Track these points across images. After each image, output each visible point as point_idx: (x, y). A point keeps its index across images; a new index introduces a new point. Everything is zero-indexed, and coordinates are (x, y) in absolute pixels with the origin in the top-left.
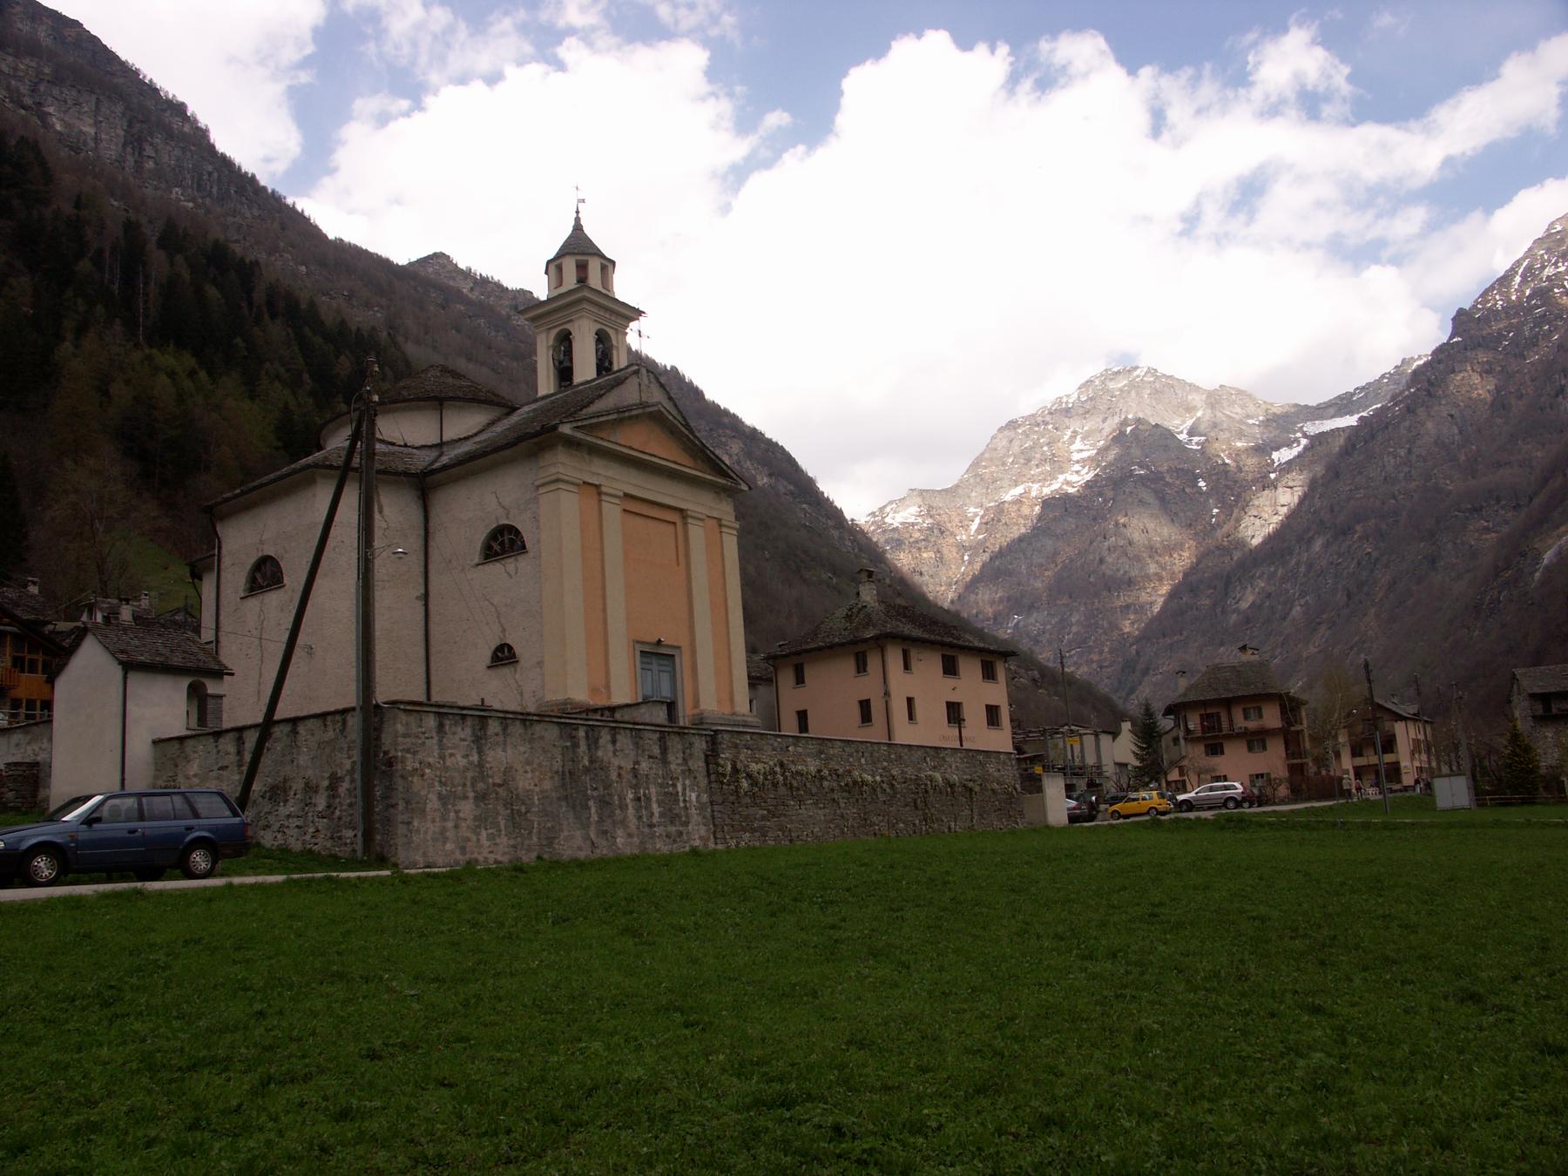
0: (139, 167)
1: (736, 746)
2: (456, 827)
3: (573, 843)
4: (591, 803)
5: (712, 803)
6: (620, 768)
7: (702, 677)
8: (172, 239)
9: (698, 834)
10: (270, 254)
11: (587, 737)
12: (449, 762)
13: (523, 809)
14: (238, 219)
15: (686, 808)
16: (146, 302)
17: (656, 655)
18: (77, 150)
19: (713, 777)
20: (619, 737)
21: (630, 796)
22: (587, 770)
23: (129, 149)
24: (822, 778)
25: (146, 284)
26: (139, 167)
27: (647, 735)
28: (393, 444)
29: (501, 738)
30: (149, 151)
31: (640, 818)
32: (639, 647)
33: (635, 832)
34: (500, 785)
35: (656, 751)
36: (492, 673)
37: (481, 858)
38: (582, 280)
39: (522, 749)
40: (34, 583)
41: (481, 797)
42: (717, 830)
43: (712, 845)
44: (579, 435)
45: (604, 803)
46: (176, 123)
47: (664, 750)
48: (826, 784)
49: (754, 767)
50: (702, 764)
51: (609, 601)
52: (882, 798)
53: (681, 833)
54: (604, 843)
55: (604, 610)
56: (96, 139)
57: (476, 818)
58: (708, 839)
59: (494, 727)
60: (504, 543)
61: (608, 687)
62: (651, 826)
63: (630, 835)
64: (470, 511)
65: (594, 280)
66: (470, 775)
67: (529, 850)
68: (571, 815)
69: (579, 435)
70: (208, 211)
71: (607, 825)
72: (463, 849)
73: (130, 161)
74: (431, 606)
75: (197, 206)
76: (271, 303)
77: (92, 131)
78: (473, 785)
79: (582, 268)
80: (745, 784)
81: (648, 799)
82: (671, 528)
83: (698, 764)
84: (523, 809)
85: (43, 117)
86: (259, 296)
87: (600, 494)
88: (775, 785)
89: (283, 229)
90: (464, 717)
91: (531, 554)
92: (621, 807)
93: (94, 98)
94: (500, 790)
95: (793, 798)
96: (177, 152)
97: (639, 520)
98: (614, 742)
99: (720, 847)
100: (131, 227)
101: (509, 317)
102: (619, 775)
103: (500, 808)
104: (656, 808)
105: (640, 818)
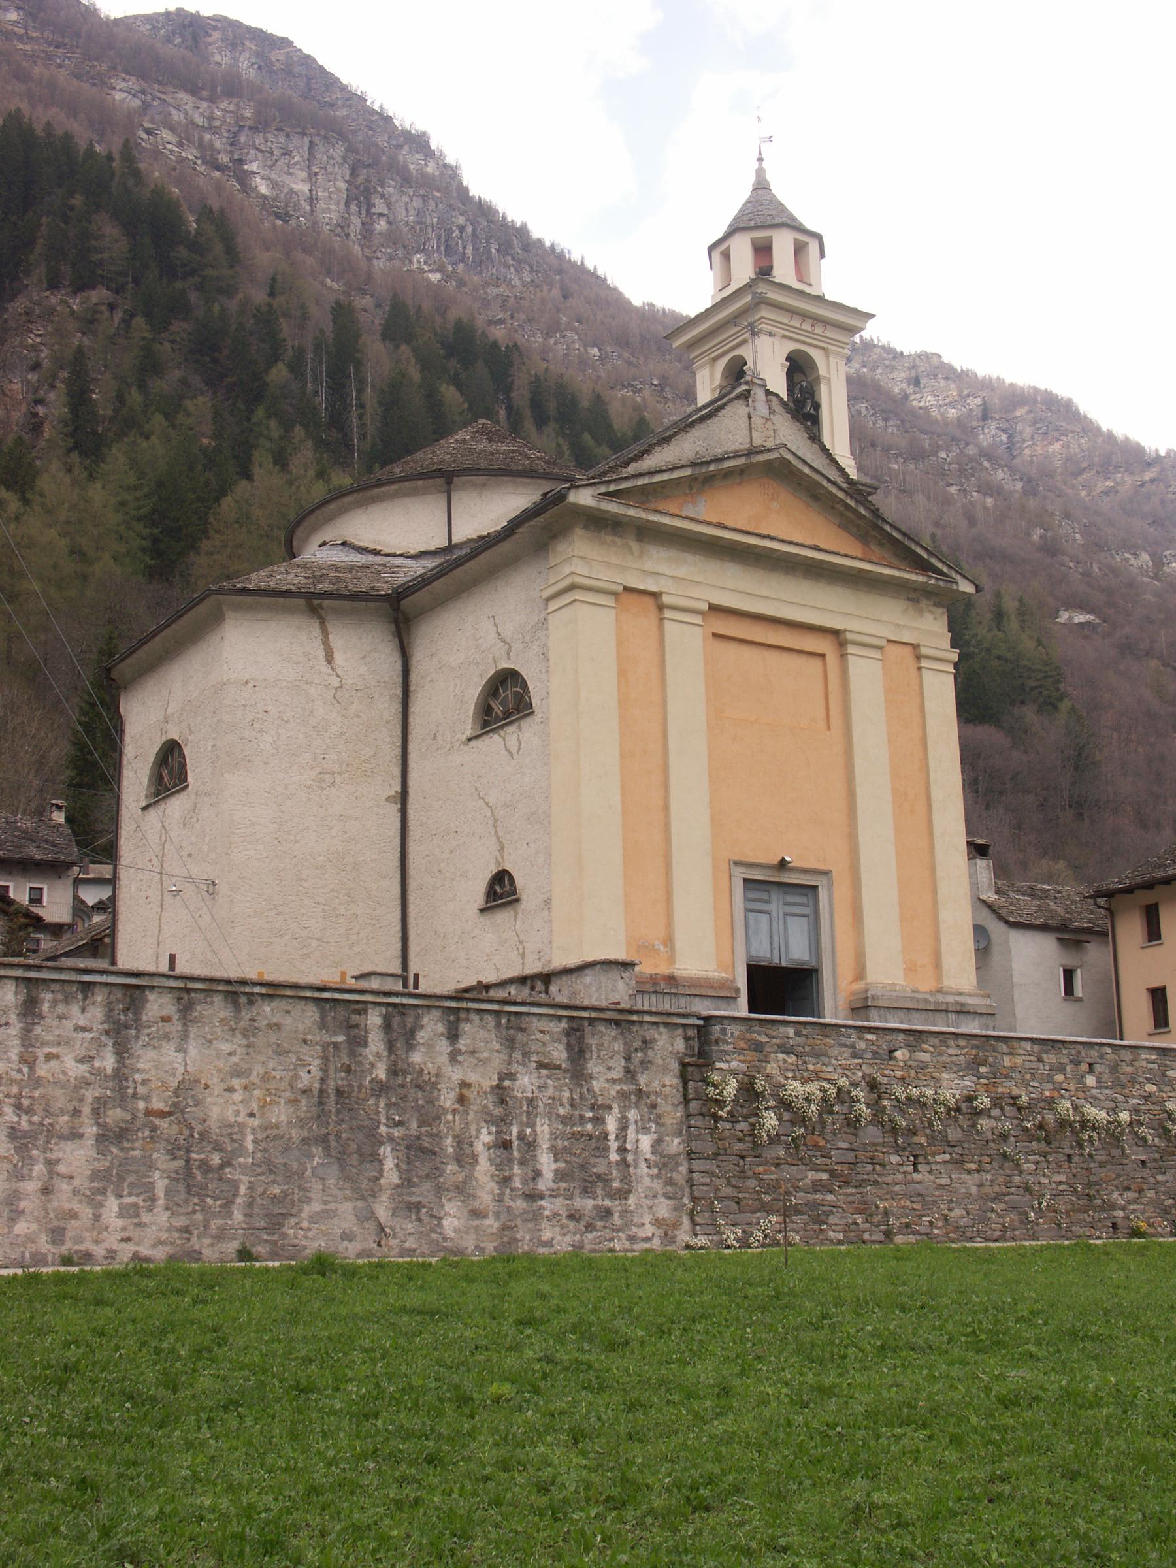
0: (367, 230)
1: (758, 1047)
2: (46, 1191)
3: (332, 1221)
4: (386, 1150)
5: (691, 1155)
6: (464, 1085)
7: (871, 923)
8: (400, 324)
9: (649, 1217)
10: (547, 335)
11: (387, 1026)
12: (42, 1070)
13: (216, 1159)
14: (503, 290)
15: (624, 1163)
16: (360, 417)
17: (777, 886)
18: (285, 217)
19: (694, 1106)
20: (466, 1027)
21: (485, 1137)
22: (381, 1089)
23: (353, 208)
24: (977, 1113)
25: (360, 391)
26: (367, 230)
27: (535, 1024)
28: (377, 553)
29: (176, 1027)
30: (380, 206)
31: (505, 1181)
32: (741, 873)
33: (492, 1206)
34: (162, 1114)
35: (559, 1054)
36: (486, 920)
37: (99, 1251)
38: (764, 271)
39: (226, 1047)
40: (59, 807)
41: (110, 1137)
42: (700, 1209)
43: (684, 1236)
44: (612, 507)
45: (419, 1152)
46: (413, 162)
47: (578, 1053)
48: (984, 1123)
49: (795, 1088)
50: (672, 1080)
51: (673, 792)
52: (1137, 1155)
53: (608, 1213)
54: (410, 1227)
55: (666, 808)
56: (312, 200)
57: (95, 1176)
58: (676, 1225)
59: (157, 1005)
60: (505, 701)
61: (669, 941)
62: (533, 1196)
63: (476, 1214)
64: (463, 647)
65: (783, 269)
66: (90, 1095)
67: (220, 1236)
68: (334, 1170)
69: (612, 507)
70: (461, 283)
71: (423, 1192)
72: (57, 1235)
73: (356, 222)
74: (411, 813)
75: (447, 277)
76: (537, 405)
77: (306, 188)
78: (96, 1112)
79: (763, 251)
80: (770, 1120)
81: (530, 1145)
82: (817, 663)
83: (663, 1081)
84: (216, 1159)
85: (244, 178)
86: (521, 395)
87: (661, 608)
88: (853, 1124)
89: (565, 297)
90: (87, 987)
91: (538, 716)
92: (459, 1160)
93: (306, 140)
94: (163, 1124)
95: (898, 1150)
96: (417, 203)
97: (746, 651)
98: (453, 1035)
99: (702, 1241)
100: (342, 313)
101: (906, 397)
102: (461, 1099)
103: (160, 1157)
104: (547, 1163)
105: (505, 1181)
